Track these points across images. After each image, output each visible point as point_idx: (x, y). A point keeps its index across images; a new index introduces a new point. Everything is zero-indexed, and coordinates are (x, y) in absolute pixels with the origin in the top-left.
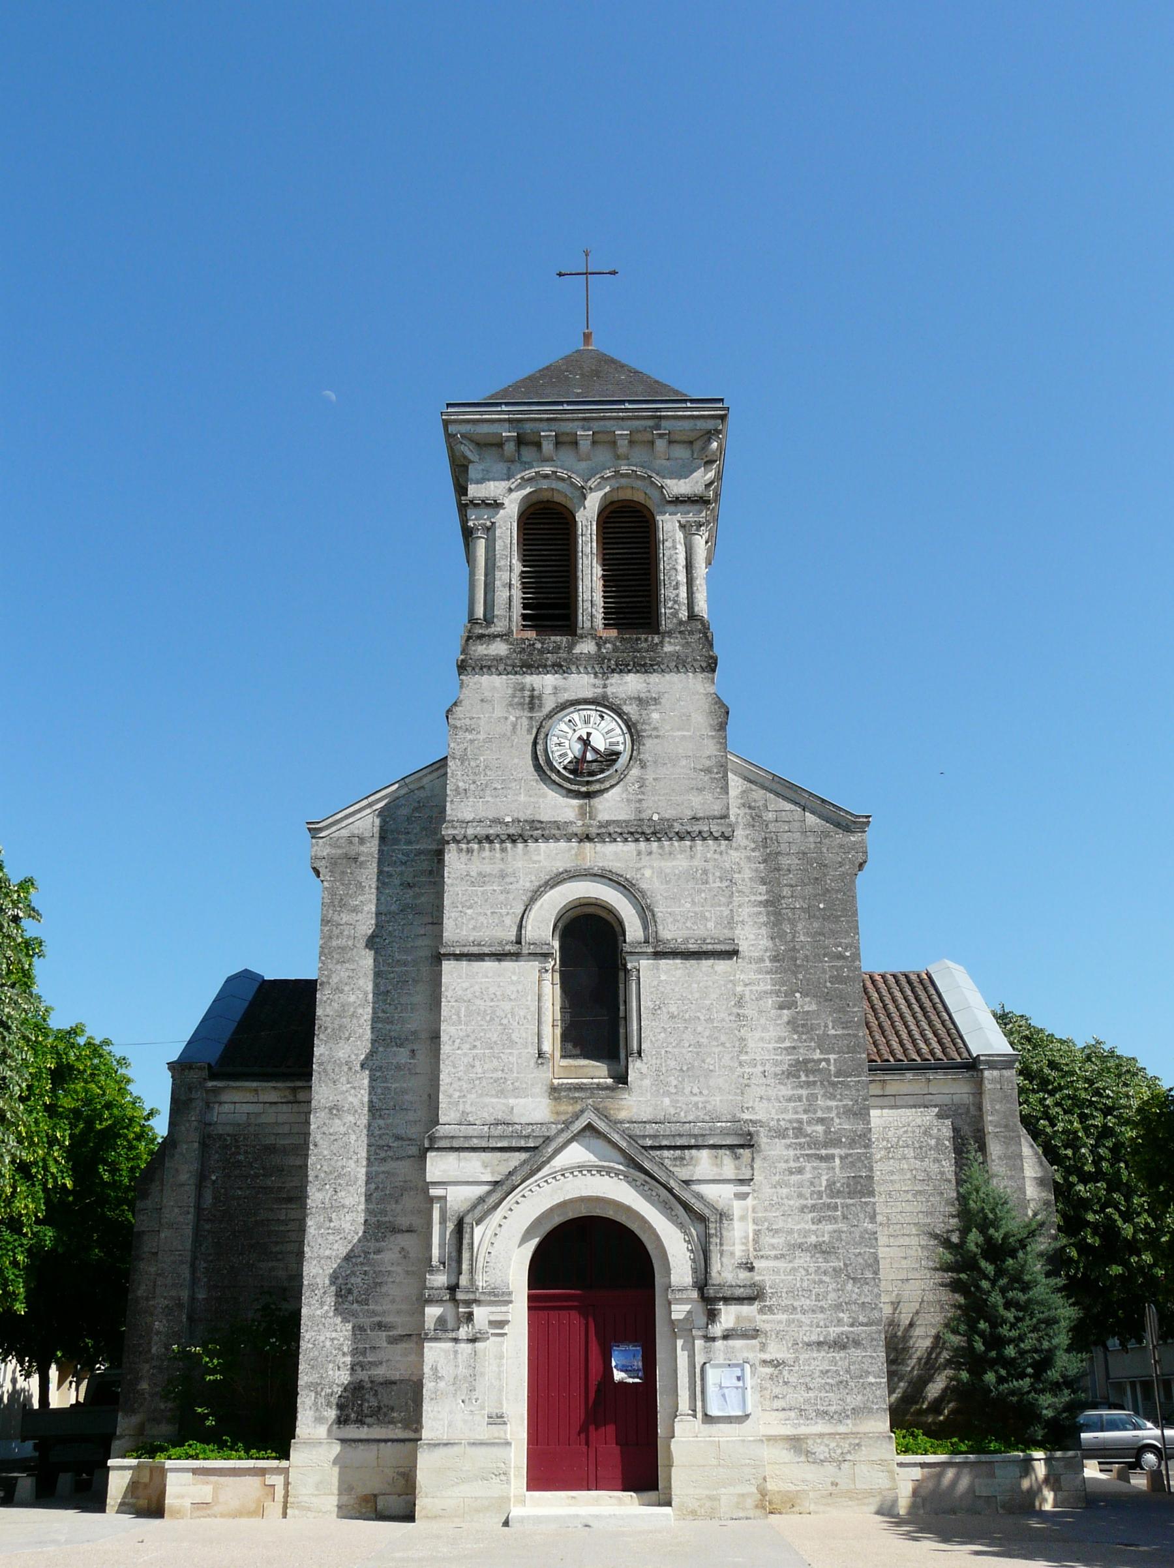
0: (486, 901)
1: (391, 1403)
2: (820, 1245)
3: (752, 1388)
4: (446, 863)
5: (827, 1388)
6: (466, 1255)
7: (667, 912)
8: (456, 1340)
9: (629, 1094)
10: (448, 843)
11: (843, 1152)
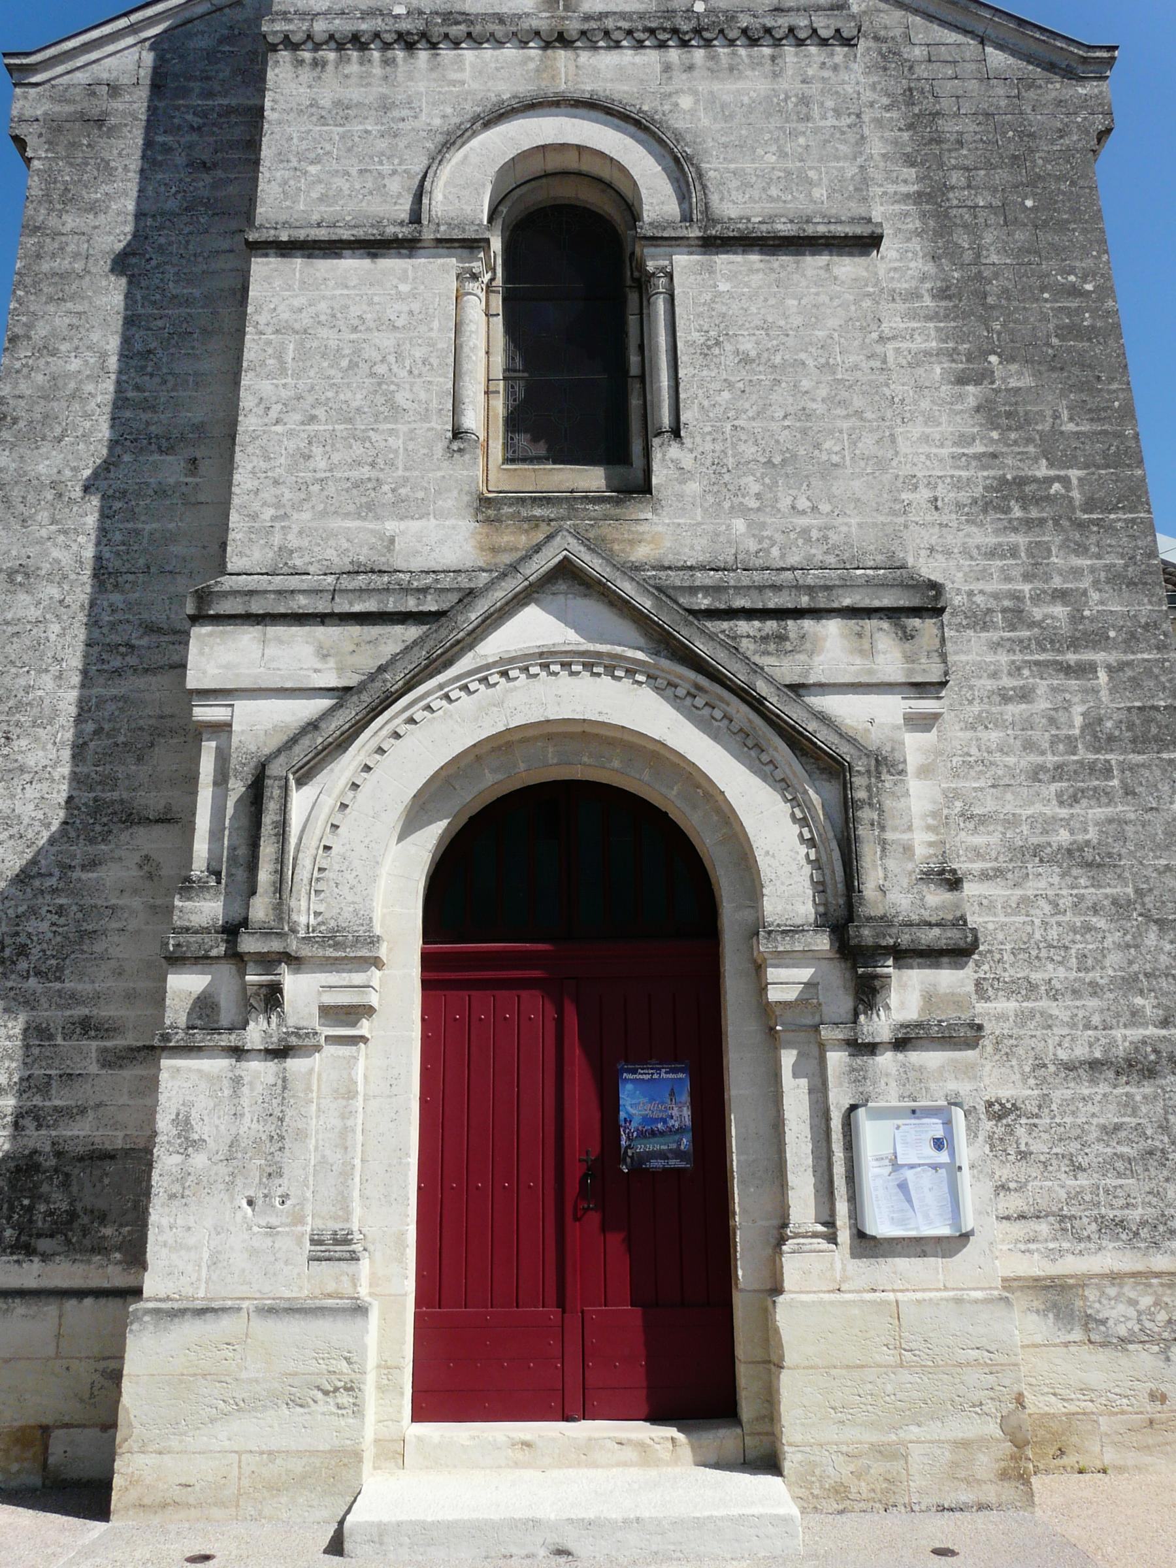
0: (349, 150)
1: (101, 1204)
2: (1081, 850)
3: (972, 1167)
4: (270, 84)
5: (1119, 1165)
6: (267, 850)
7: (728, 170)
8: (238, 1052)
9: (654, 511)
10: (274, 48)
11: (1113, 657)
